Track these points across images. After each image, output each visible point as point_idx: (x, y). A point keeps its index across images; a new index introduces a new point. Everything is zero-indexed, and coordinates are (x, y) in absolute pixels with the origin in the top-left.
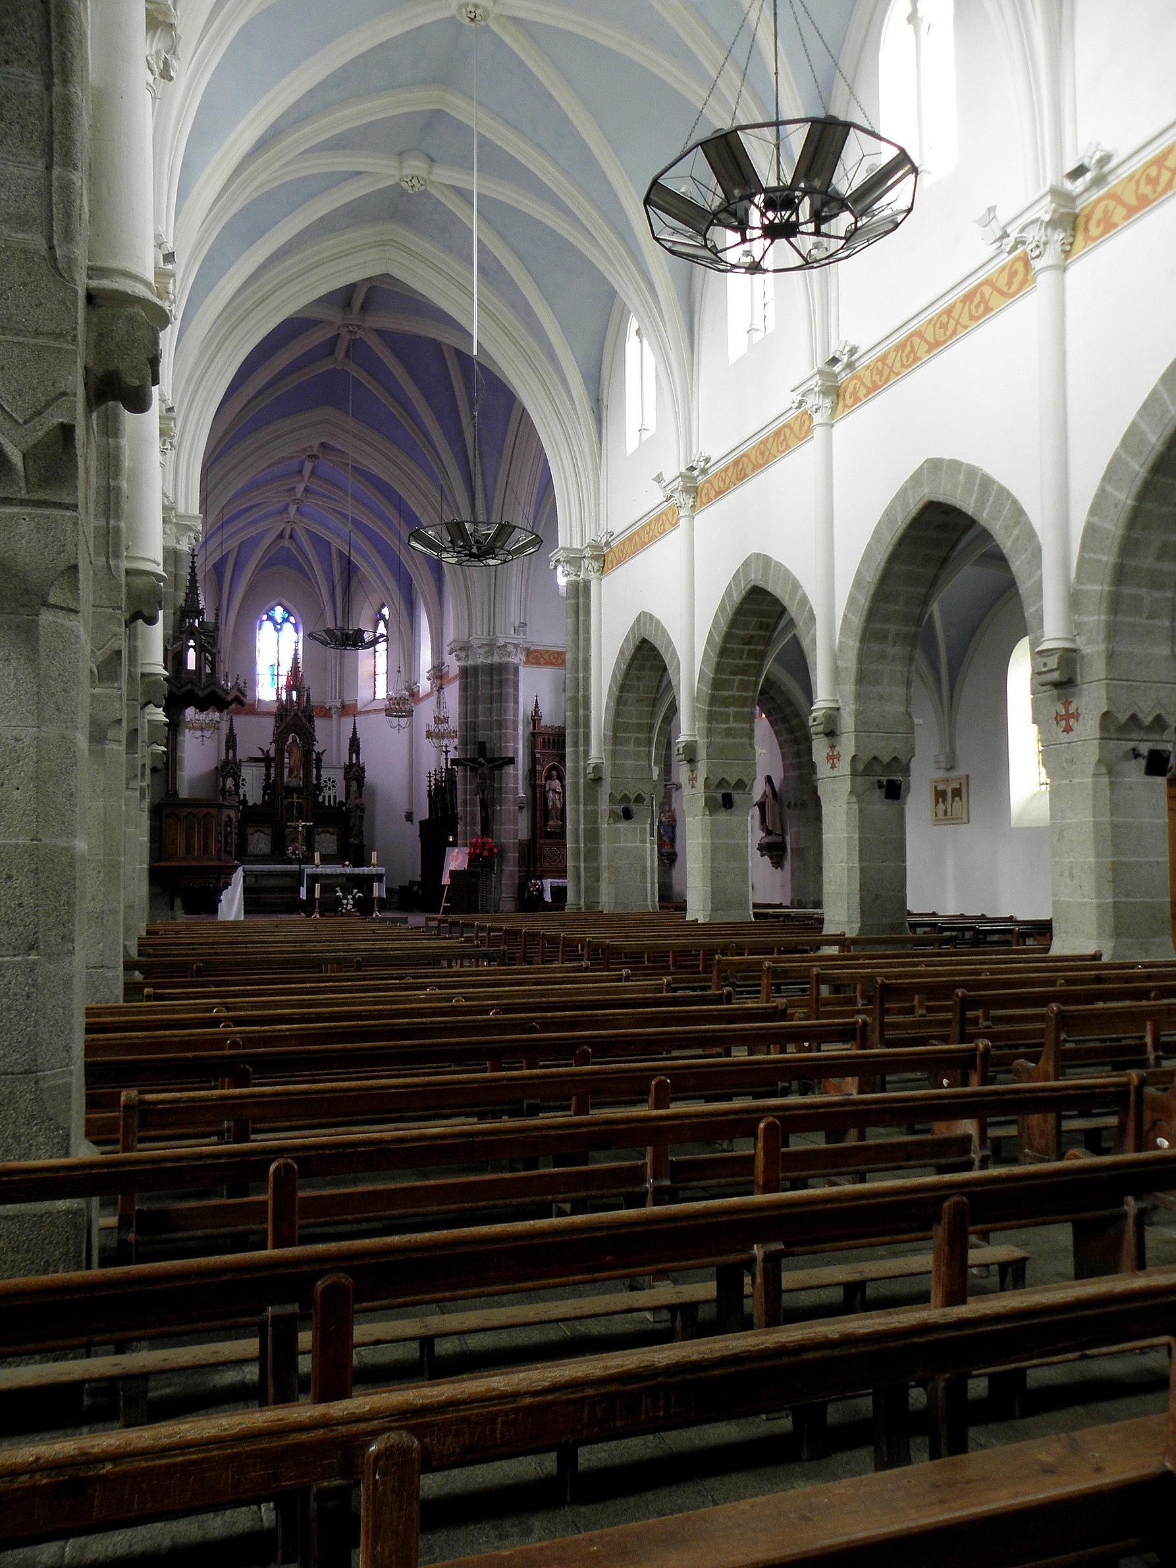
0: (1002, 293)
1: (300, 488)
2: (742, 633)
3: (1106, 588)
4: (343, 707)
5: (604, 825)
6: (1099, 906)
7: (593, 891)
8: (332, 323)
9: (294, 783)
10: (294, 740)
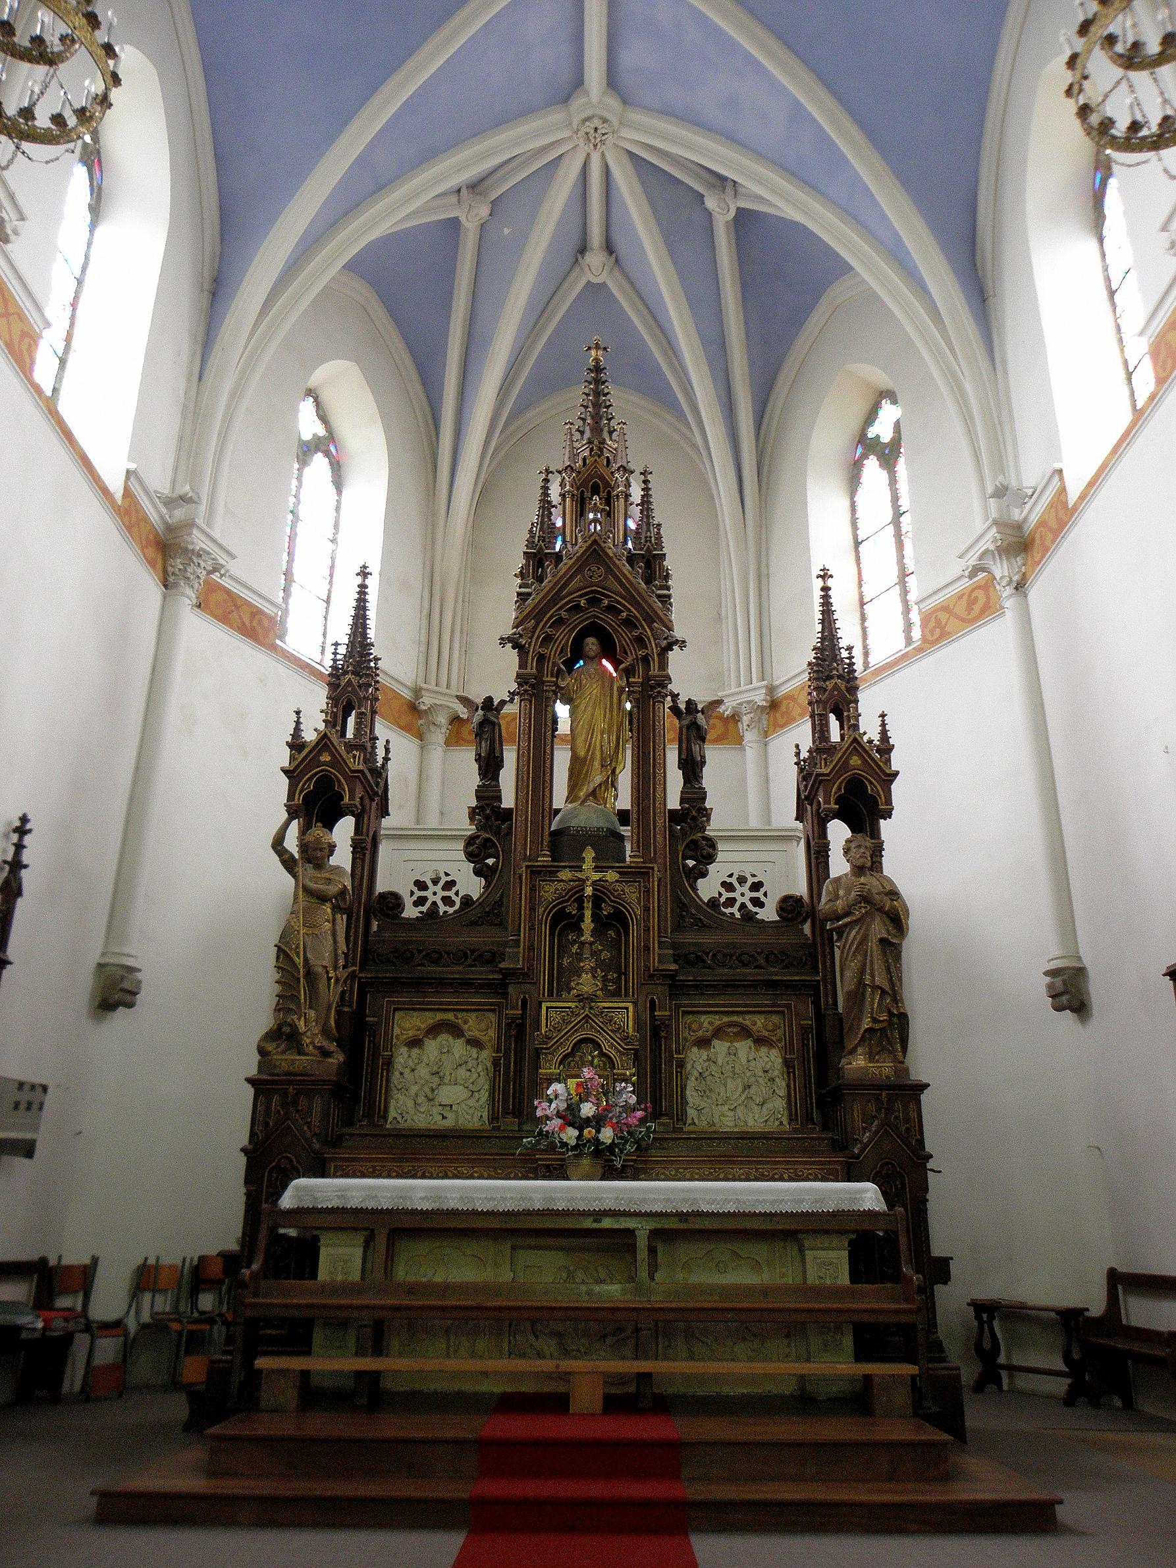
9: (589, 817)
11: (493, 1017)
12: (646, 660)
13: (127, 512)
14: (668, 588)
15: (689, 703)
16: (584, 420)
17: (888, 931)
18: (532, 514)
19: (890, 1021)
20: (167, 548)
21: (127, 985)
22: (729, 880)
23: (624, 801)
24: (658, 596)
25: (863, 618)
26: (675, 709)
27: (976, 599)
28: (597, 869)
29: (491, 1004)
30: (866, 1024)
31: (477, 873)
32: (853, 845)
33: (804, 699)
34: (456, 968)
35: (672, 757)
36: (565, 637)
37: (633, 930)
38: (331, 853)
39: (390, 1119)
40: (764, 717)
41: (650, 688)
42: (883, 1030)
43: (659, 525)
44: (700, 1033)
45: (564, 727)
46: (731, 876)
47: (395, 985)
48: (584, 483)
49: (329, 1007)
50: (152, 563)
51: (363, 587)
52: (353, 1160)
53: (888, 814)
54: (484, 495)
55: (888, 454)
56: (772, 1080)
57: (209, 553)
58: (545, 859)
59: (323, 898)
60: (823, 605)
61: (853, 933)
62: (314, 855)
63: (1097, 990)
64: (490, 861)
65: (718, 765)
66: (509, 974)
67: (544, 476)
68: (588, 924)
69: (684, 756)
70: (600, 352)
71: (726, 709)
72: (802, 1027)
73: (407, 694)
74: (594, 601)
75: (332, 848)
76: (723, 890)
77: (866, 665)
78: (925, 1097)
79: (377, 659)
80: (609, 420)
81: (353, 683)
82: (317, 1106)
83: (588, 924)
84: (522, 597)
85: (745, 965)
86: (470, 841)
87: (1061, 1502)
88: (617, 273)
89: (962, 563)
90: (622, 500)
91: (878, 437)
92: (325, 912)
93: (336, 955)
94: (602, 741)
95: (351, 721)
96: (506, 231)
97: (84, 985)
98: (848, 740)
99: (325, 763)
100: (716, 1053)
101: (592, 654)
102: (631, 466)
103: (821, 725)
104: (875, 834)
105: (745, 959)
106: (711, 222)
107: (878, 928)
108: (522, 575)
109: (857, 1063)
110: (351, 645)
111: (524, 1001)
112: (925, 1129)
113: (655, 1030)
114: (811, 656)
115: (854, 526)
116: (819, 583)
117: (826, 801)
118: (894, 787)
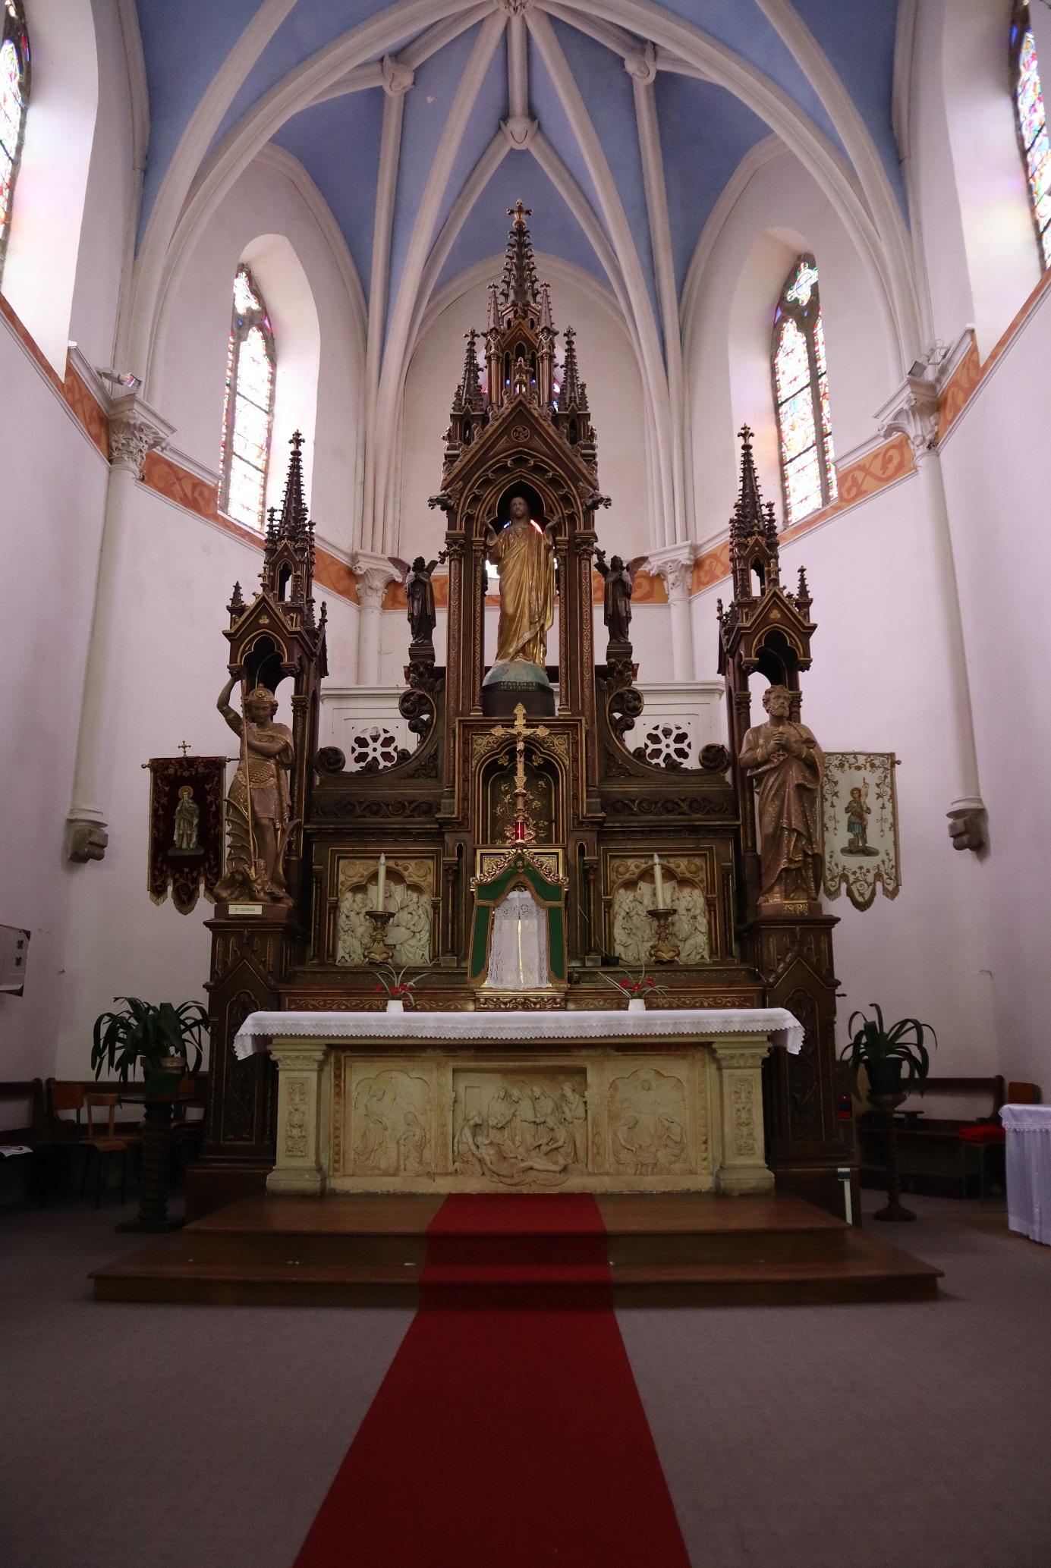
0: (877, 478)
9: (520, 673)
11: (430, 863)
12: (572, 518)
13: (72, 390)
14: (593, 448)
15: (616, 560)
16: (508, 283)
17: (804, 777)
18: (458, 377)
19: (804, 861)
20: (107, 419)
21: (95, 839)
22: (654, 732)
23: (553, 658)
24: (583, 455)
25: (784, 478)
26: (601, 566)
27: (891, 459)
28: (527, 726)
29: (428, 851)
30: (783, 864)
31: (413, 728)
32: (772, 696)
33: (726, 557)
34: (395, 819)
35: (599, 614)
36: (492, 497)
37: (563, 780)
38: (274, 712)
39: (339, 958)
40: (689, 576)
41: (577, 546)
42: (798, 869)
43: (583, 386)
44: (627, 876)
45: (493, 589)
46: (656, 728)
47: (340, 835)
48: (509, 346)
49: (278, 856)
50: (96, 439)
51: (296, 454)
52: (304, 994)
53: (806, 666)
54: (413, 363)
55: (806, 317)
56: (694, 917)
57: (149, 427)
58: (477, 714)
59: (267, 755)
60: (744, 463)
61: (772, 780)
62: (259, 713)
63: (995, 830)
64: (425, 717)
65: (642, 621)
66: (444, 823)
67: (469, 339)
68: (520, 778)
69: (610, 611)
70: (523, 216)
71: (651, 567)
72: (723, 869)
73: (345, 560)
74: (520, 461)
75: (274, 707)
76: (649, 743)
77: (786, 522)
78: (836, 931)
79: (311, 524)
80: (533, 282)
81: (289, 545)
82: (270, 949)
83: (520, 778)
84: (450, 459)
85: (669, 812)
86: (405, 698)
87: (942, 1275)
88: (539, 139)
89: (878, 423)
90: (546, 362)
91: (797, 300)
92: (270, 767)
93: (282, 808)
94: (530, 598)
95: (289, 585)
96: (430, 100)
97: (57, 838)
98: (768, 595)
99: (264, 626)
100: (642, 895)
101: (519, 513)
102: (555, 327)
103: (742, 579)
104: (794, 685)
105: (669, 805)
106: (632, 87)
107: (795, 775)
108: (449, 437)
109: (774, 900)
110: (286, 510)
111: (460, 848)
112: (835, 960)
113: (585, 872)
114: (732, 513)
115: (775, 388)
116: (741, 441)
117: (747, 654)
118: (813, 640)
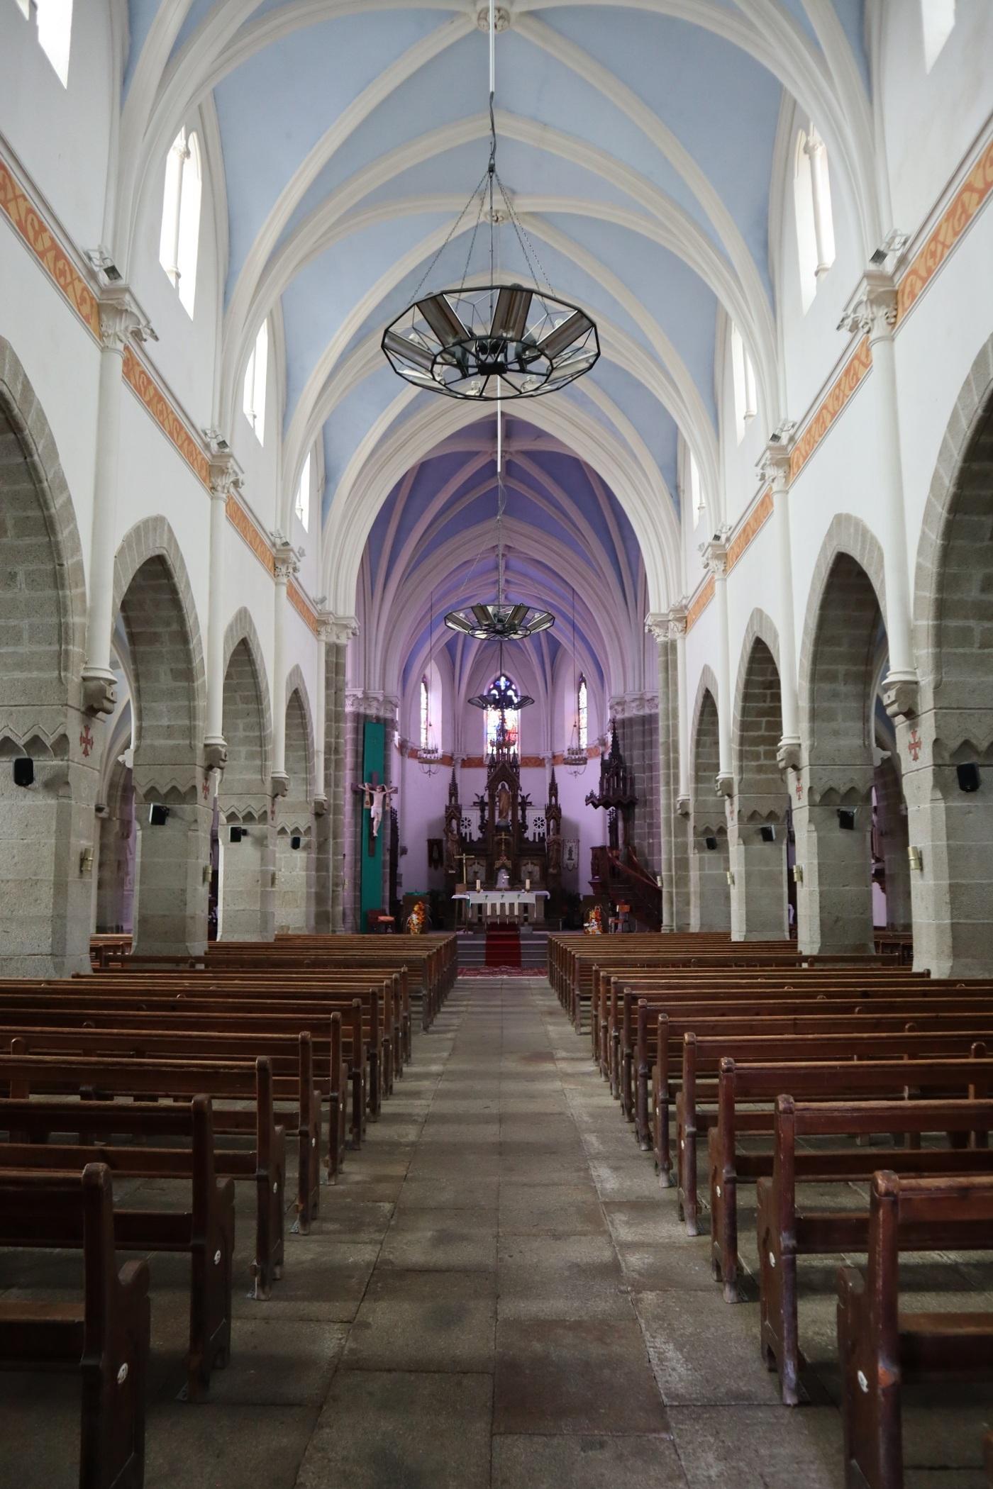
1: (502, 582)
2: (760, 679)
3: (931, 623)
4: (554, 757)
5: (693, 856)
6: (938, 926)
7: (684, 914)
8: (486, 453)
9: (503, 824)
10: (503, 787)
